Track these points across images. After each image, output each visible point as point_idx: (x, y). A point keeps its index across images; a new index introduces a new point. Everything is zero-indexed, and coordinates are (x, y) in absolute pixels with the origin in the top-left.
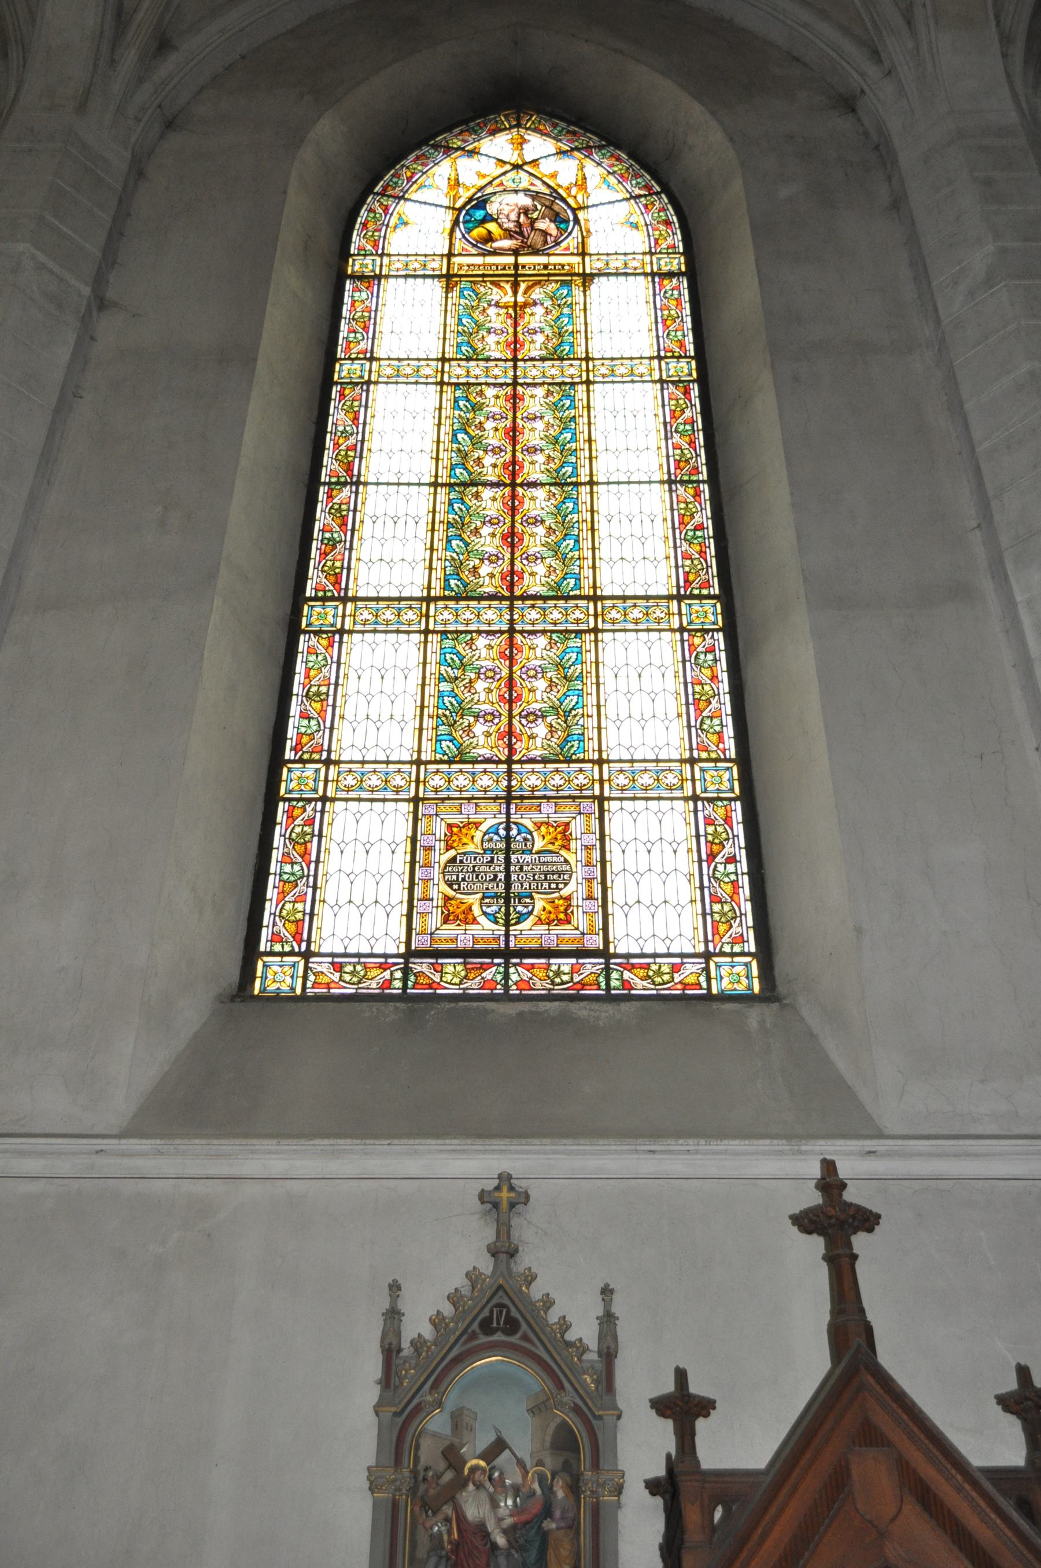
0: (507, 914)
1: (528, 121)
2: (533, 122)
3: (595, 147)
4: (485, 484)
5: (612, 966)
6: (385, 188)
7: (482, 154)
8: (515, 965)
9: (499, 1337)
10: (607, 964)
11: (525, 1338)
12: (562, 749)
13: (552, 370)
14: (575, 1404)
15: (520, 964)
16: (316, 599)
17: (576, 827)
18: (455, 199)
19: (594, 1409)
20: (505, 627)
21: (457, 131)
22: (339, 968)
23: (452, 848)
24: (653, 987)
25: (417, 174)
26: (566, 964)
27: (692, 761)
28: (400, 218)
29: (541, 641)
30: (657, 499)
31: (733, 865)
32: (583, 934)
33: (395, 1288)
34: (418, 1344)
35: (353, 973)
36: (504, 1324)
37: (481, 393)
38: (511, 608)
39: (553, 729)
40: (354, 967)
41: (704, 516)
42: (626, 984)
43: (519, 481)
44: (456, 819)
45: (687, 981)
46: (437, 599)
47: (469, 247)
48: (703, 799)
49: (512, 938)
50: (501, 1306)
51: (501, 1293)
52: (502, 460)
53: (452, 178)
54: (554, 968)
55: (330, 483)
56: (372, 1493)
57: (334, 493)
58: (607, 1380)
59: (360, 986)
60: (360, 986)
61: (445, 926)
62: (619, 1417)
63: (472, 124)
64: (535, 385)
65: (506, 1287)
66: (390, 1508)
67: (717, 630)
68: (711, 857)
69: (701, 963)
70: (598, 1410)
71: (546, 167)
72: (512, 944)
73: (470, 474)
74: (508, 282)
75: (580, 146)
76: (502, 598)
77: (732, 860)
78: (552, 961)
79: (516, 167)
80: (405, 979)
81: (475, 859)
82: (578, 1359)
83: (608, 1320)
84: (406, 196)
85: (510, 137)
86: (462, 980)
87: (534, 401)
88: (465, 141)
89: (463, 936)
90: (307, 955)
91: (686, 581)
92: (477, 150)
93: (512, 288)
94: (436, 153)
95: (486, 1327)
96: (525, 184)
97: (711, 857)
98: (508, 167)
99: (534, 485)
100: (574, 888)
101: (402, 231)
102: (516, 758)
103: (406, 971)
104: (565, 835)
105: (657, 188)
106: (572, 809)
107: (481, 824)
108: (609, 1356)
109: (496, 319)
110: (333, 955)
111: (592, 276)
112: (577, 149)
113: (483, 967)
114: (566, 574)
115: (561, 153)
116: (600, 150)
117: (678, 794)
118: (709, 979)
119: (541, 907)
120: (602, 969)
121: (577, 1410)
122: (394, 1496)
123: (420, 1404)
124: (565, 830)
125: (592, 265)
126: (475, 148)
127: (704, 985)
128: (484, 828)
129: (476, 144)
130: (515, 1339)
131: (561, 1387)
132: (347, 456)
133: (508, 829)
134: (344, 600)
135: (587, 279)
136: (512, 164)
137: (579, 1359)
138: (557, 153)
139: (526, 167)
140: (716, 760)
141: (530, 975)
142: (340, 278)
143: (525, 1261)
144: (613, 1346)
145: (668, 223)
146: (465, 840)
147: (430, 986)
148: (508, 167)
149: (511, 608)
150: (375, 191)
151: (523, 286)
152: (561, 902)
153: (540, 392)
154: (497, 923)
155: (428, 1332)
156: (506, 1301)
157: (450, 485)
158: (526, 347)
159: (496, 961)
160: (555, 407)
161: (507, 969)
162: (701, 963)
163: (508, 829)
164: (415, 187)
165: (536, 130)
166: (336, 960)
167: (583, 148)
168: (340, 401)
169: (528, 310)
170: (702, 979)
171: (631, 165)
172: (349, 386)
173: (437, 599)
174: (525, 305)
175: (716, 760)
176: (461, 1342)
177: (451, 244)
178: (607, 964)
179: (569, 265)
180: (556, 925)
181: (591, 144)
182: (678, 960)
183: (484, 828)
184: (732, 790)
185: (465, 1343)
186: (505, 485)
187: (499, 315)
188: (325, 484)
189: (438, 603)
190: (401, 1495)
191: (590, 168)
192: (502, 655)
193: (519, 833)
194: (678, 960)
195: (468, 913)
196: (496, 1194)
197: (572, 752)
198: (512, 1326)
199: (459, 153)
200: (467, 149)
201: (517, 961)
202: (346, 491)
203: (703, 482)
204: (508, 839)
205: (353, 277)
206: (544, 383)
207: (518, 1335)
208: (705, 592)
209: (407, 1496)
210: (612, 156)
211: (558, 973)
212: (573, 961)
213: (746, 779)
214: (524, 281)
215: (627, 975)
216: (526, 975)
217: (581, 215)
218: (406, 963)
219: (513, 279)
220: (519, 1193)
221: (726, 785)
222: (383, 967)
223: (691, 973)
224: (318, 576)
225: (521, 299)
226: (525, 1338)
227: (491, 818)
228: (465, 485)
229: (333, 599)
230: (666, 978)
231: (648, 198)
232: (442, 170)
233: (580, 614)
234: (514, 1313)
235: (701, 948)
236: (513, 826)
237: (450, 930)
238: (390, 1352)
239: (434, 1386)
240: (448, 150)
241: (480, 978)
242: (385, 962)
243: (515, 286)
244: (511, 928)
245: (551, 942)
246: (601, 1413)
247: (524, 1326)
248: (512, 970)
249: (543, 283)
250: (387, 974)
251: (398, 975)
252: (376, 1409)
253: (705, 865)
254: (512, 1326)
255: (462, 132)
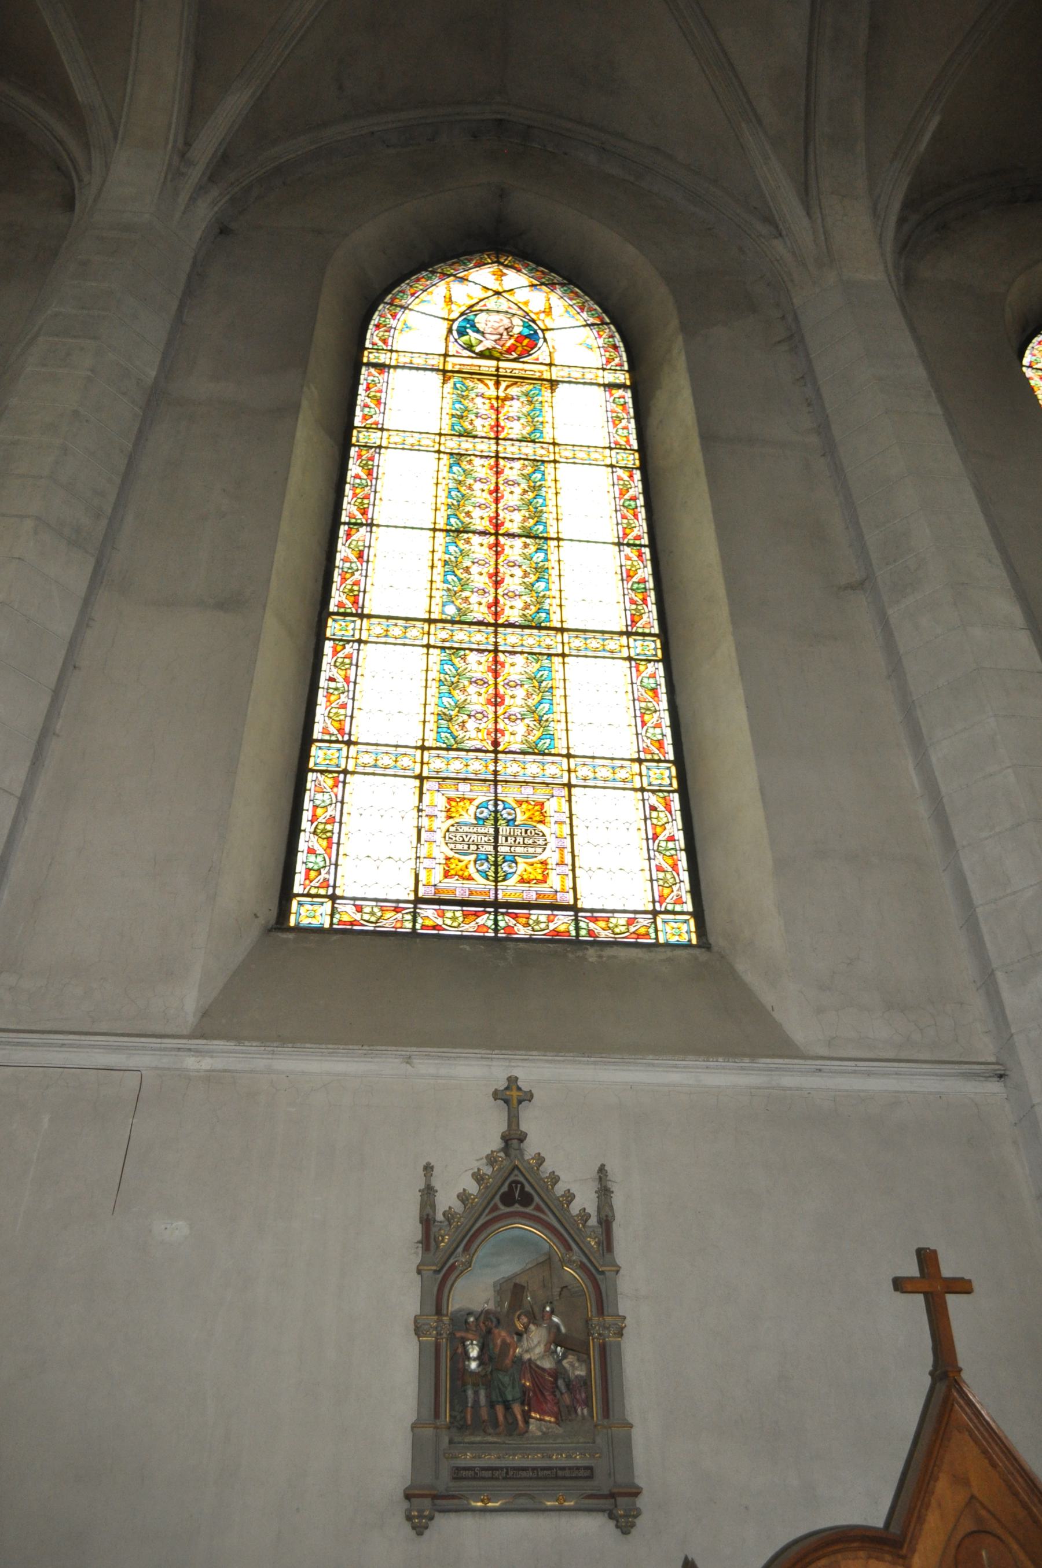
0: (496, 872)
1: (506, 260)
2: (510, 262)
3: (558, 284)
4: (474, 532)
5: (579, 918)
6: (393, 299)
7: (470, 281)
8: (503, 914)
9: (517, 1208)
10: (576, 916)
11: (538, 1208)
12: (537, 745)
13: (528, 449)
14: (581, 1262)
15: (507, 914)
16: (338, 614)
17: (551, 806)
18: (450, 311)
19: (597, 1265)
20: (491, 648)
21: (450, 262)
22: (359, 909)
23: (451, 817)
24: (613, 936)
25: (418, 291)
26: (542, 915)
27: (640, 761)
28: (405, 324)
29: (519, 659)
30: (611, 559)
31: (673, 842)
32: (556, 892)
33: (428, 1168)
34: (449, 1215)
35: (372, 914)
36: (519, 1197)
37: (470, 462)
38: (496, 633)
39: (530, 729)
40: (372, 908)
41: (646, 572)
42: (590, 933)
43: (501, 532)
44: (452, 794)
45: (639, 932)
46: (436, 621)
47: (460, 349)
48: (648, 791)
49: (500, 892)
50: (517, 1182)
51: (516, 1172)
52: (487, 514)
53: (448, 297)
54: (534, 917)
55: (349, 523)
56: (419, 1338)
57: (353, 532)
58: (607, 1243)
59: (378, 925)
60: (378, 925)
61: (447, 880)
62: (617, 1272)
63: (462, 258)
64: (513, 459)
65: (520, 1166)
66: (433, 1349)
67: (658, 661)
68: (655, 837)
69: (571, 916)
70: (602, 1266)
71: (521, 296)
72: (500, 896)
73: (462, 523)
74: (491, 380)
75: (547, 282)
76: (488, 625)
77: (671, 839)
78: (532, 912)
79: (497, 293)
80: (414, 921)
81: (526, 831)
82: (582, 1224)
83: (604, 1192)
84: (410, 307)
85: (491, 270)
86: (460, 924)
87: (512, 471)
88: (455, 270)
89: (459, 889)
90: (333, 898)
91: (633, 621)
92: (465, 277)
93: (494, 385)
94: (434, 277)
95: (508, 1199)
96: (504, 308)
97: (655, 837)
98: (491, 293)
99: (513, 536)
100: (551, 855)
101: (406, 334)
102: (500, 749)
103: (415, 916)
104: (542, 813)
105: (607, 320)
106: (515, 790)
107: (474, 799)
108: (606, 1223)
109: (482, 406)
110: (355, 899)
111: (557, 382)
112: (542, 284)
113: (477, 915)
114: (539, 609)
115: (533, 285)
116: (562, 287)
117: (629, 785)
118: (656, 931)
119: (523, 869)
120: (572, 920)
121: (582, 1267)
122: (437, 1339)
123: (453, 1265)
124: (542, 808)
125: (556, 374)
126: (465, 275)
127: (653, 936)
128: (476, 803)
129: (466, 273)
130: (529, 1210)
131: (569, 1248)
132: (362, 503)
133: (496, 805)
134: (362, 616)
135: (553, 384)
136: (494, 291)
137: (584, 1226)
138: (529, 286)
139: (503, 294)
140: (659, 761)
141: (515, 922)
142: (357, 365)
143: (531, 1148)
144: (610, 1214)
145: (615, 347)
146: (462, 812)
147: (434, 927)
148: (491, 293)
149: (496, 633)
150: (386, 301)
151: (503, 385)
152: (540, 865)
153: (517, 465)
154: (488, 879)
155: (458, 1207)
156: (521, 1179)
157: (447, 531)
158: (506, 430)
159: (488, 909)
160: (528, 477)
161: (496, 916)
162: (571, 916)
163: (496, 805)
164: (417, 300)
165: (512, 267)
166: (358, 903)
167: (549, 284)
168: (357, 460)
169: (507, 403)
170: (651, 930)
171: (587, 301)
172: (365, 449)
173: (436, 621)
174: (506, 399)
175: (659, 761)
176: (487, 1211)
177: (447, 346)
178: (576, 916)
179: (539, 372)
180: (535, 883)
181: (555, 281)
182: (632, 916)
183: (476, 803)
184: (671, 785)
185: (490, 1213)
186: (491, 534)
187: (484, 404)
188: (345, 523)
189: (660, 665)
190: (442, 1339)
191: (554, 298)
192: (489, 669)
193: (504, 808)
194: (632, 916)
195: (464, 871)
196: (508, 1093)
197: (545, 747)
198: (526, 1199)
199: (452, 278)
200: (458, 275)
201: (504, 910)
202: (363, 530)
203: (645, 546)
204: (496, 812)
205: (369, 364)
206: (520, 459)
207: (532, 1207)
208: (647, 631)
209: (447, 1340)
210: (572, 292)
211: (538, 922)
212: (549, 912)
213: (682, 777)
214: (504, 381)
215: (592, 926)
216: (512, 922)
217: (548, 334)
218: (415, 908)
219: (495, 378)
220: (525, 1092)
221: (667, 781)
222: (397, 910)
223: (563, 923)
224: (340, 596)
225: (502, 394)
226: (538, 1208)
227: (482, 794)
228: (458, 531)
229: (351, 615)
230: (543, 926)
231: (601, 326)
232: (440, 289)
233: (552, 641)
234: (528, 1188)
235: (650, 907)
236: (499, 802)
237: (452, 883)
238: (427, 1221)
239: (466, 1249)
240: (445, 275)
241: (474, 922)
242: (397, 906)
243: (497, 384)
244: (499, 884)
245: (531, 897)
246: (603, 1269)
247: (537, 1199)
248: (500, 918)
249: (519, 383)
250: (399, 916)
251: (409, 917)
252: (420, 1268)
253: (651, 842)
254: (526, 1199)
255: (453, 264)
